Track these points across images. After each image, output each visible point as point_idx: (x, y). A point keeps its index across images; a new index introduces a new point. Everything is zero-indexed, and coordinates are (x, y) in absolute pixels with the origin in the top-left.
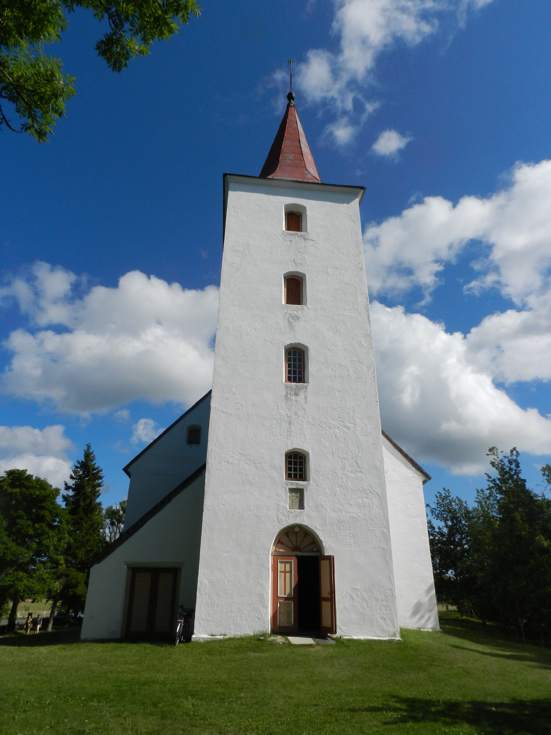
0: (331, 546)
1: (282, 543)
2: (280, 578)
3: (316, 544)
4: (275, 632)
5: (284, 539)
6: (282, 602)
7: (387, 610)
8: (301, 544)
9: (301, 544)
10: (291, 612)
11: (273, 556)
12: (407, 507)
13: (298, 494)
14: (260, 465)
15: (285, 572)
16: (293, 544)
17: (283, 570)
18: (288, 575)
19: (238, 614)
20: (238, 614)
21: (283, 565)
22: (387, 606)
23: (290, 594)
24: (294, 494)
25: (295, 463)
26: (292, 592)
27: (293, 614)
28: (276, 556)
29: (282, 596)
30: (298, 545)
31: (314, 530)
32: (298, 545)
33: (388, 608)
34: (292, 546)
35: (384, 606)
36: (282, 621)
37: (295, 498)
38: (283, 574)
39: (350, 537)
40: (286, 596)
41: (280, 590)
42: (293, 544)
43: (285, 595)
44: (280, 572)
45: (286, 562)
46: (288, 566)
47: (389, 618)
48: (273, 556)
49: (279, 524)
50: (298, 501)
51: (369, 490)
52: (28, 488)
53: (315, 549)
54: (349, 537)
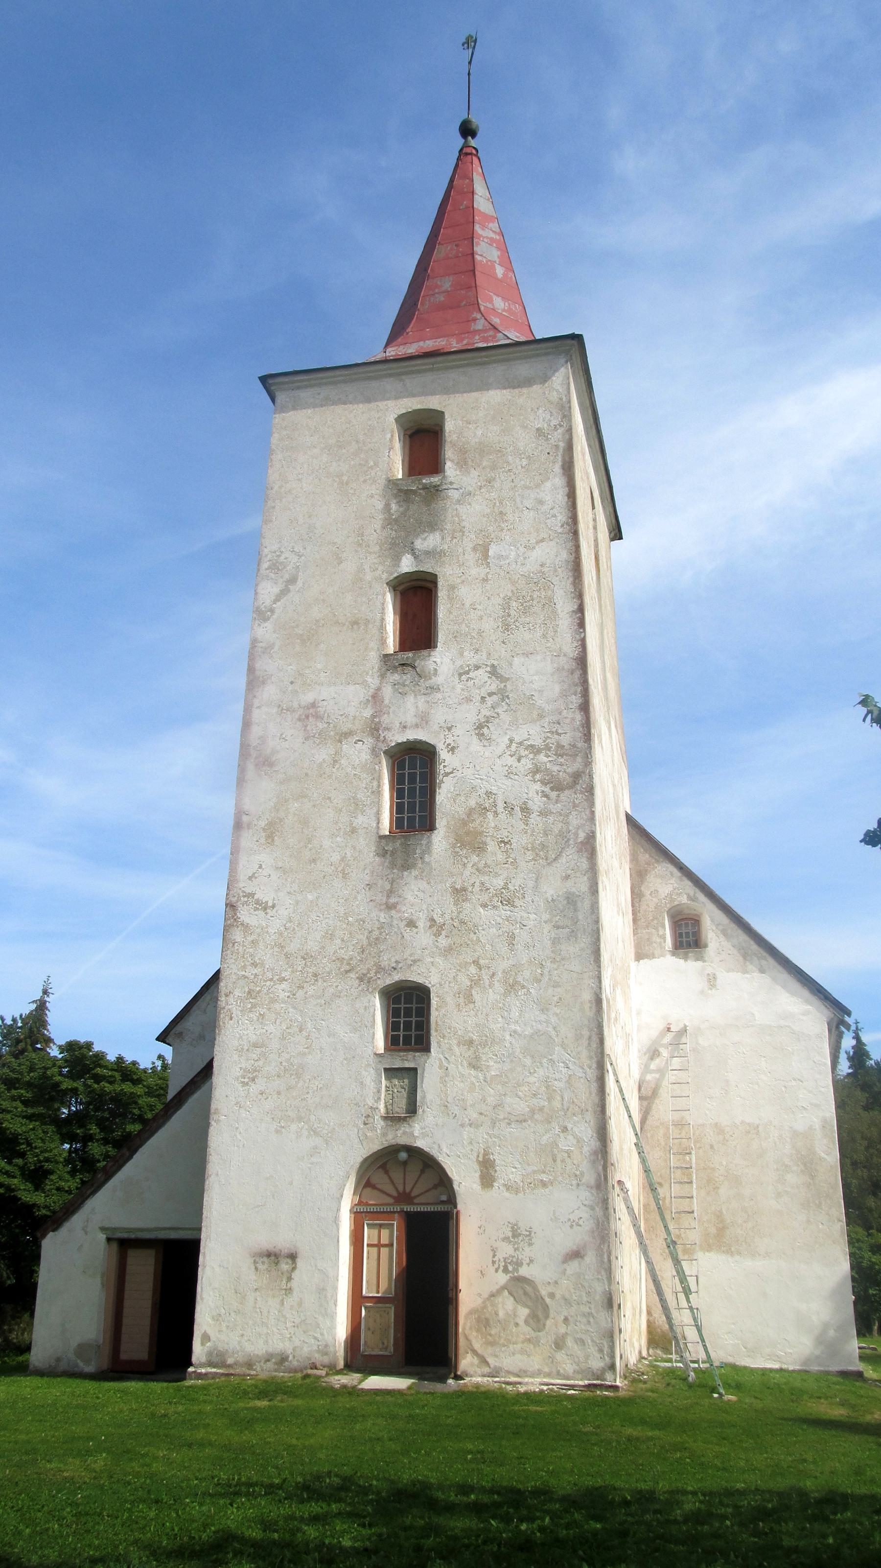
0: (472, 1189)
1: (374, 1187)
2: (368, 1258)
3: (446, 1187)
4: (350, 1367)
5: (380, 1179)
6: (370, 1307)
7: (589, 1322)
8: (404, 1184)
9: (404, 1184)
10: (389, 1327)
11: (355, 1213)
12: (785, 1087)
13: (406, 1081)
14: (323, 1022)
15: (379, 1246)
16: (397, 1189)
17: (376, 1242)
18: (384, 1251)
19: (275, 1329)
20: (275, 1329)
21: (376, 1232)
22: (590, 1314)
23: (388, 1290)
24: (396, 1082)
25: (408, 1013)
26: (391, 1289)
27: (392, 1331)
28: (359, 1217)
29: (371, 1295)
30: (408, 1190)
31: (435, 1156)
32: (408, 1190)
33: (591, 1320)
34: (395, 1194)
35: (584, 1315)
36: (369, 1344)
37: (400, 1089)
38: (375, 1249)
39: (516, 1168)
40: (379, 1295)
41: (367, 1282)
42: (397, 1189)
43: (378, 1292)
44: (368, 1245)
45: (381, 1226)
46: (385, 1233)
47: (593, 1341)
48: (355, 1213)
49: (361, 1146)
50: (405, 1096)
51: (563, 1063)
52: (98, 1079)
53: (444, 1198)
54: (514, 1170)
